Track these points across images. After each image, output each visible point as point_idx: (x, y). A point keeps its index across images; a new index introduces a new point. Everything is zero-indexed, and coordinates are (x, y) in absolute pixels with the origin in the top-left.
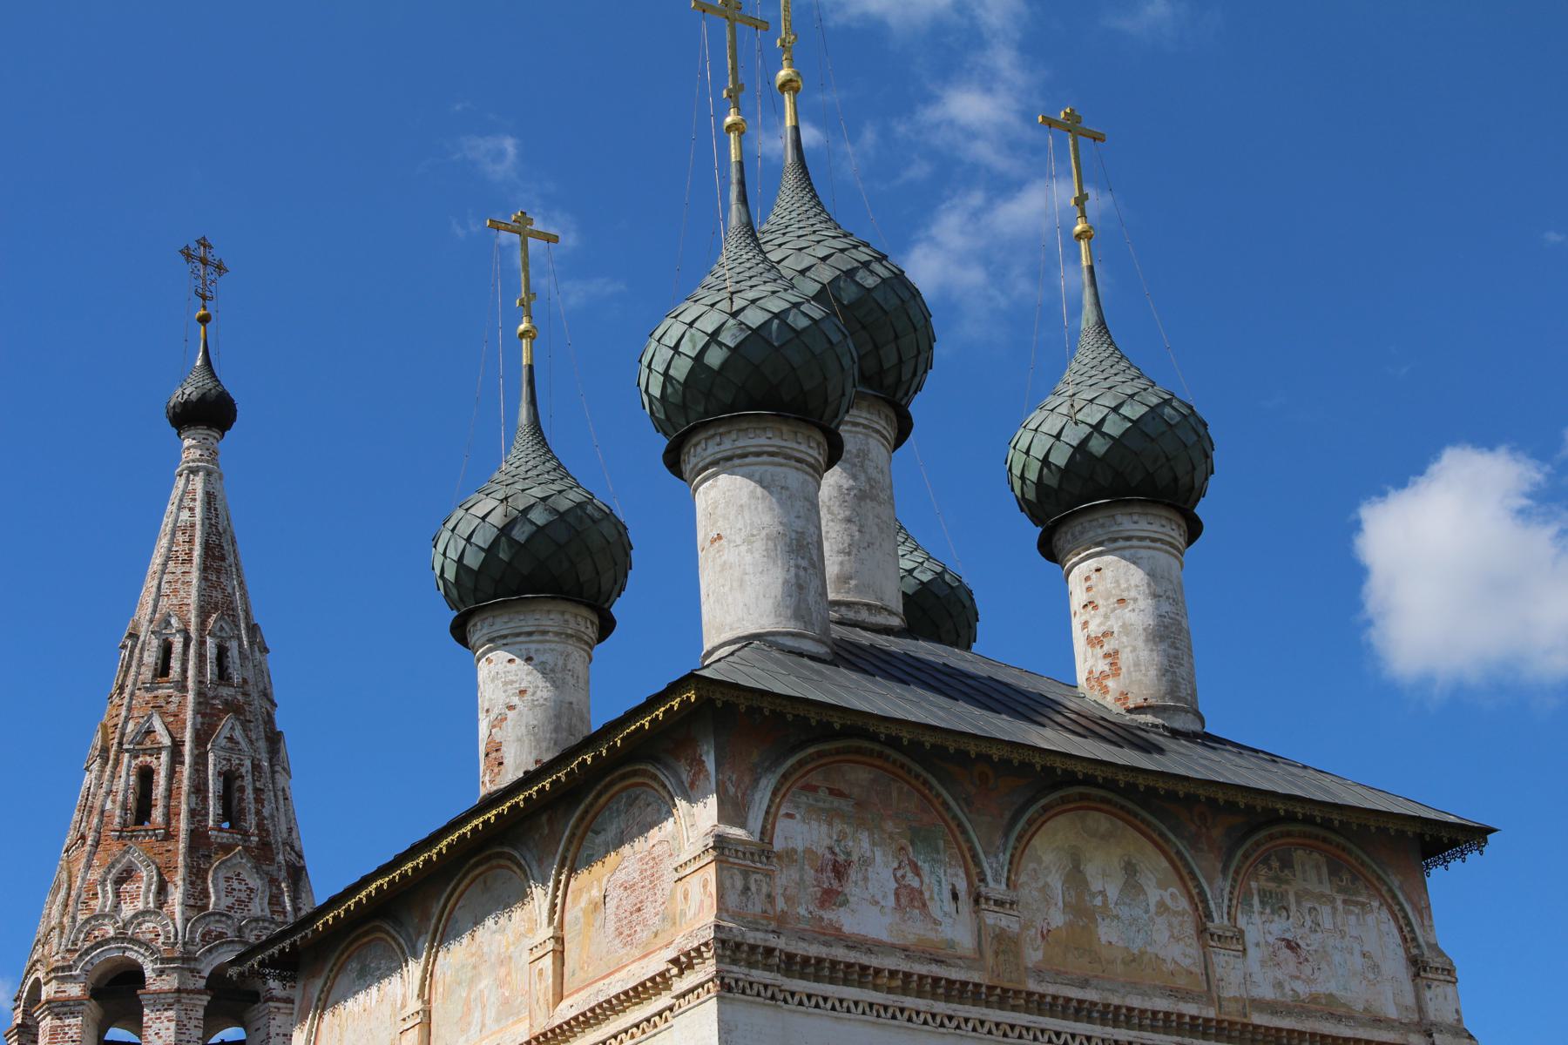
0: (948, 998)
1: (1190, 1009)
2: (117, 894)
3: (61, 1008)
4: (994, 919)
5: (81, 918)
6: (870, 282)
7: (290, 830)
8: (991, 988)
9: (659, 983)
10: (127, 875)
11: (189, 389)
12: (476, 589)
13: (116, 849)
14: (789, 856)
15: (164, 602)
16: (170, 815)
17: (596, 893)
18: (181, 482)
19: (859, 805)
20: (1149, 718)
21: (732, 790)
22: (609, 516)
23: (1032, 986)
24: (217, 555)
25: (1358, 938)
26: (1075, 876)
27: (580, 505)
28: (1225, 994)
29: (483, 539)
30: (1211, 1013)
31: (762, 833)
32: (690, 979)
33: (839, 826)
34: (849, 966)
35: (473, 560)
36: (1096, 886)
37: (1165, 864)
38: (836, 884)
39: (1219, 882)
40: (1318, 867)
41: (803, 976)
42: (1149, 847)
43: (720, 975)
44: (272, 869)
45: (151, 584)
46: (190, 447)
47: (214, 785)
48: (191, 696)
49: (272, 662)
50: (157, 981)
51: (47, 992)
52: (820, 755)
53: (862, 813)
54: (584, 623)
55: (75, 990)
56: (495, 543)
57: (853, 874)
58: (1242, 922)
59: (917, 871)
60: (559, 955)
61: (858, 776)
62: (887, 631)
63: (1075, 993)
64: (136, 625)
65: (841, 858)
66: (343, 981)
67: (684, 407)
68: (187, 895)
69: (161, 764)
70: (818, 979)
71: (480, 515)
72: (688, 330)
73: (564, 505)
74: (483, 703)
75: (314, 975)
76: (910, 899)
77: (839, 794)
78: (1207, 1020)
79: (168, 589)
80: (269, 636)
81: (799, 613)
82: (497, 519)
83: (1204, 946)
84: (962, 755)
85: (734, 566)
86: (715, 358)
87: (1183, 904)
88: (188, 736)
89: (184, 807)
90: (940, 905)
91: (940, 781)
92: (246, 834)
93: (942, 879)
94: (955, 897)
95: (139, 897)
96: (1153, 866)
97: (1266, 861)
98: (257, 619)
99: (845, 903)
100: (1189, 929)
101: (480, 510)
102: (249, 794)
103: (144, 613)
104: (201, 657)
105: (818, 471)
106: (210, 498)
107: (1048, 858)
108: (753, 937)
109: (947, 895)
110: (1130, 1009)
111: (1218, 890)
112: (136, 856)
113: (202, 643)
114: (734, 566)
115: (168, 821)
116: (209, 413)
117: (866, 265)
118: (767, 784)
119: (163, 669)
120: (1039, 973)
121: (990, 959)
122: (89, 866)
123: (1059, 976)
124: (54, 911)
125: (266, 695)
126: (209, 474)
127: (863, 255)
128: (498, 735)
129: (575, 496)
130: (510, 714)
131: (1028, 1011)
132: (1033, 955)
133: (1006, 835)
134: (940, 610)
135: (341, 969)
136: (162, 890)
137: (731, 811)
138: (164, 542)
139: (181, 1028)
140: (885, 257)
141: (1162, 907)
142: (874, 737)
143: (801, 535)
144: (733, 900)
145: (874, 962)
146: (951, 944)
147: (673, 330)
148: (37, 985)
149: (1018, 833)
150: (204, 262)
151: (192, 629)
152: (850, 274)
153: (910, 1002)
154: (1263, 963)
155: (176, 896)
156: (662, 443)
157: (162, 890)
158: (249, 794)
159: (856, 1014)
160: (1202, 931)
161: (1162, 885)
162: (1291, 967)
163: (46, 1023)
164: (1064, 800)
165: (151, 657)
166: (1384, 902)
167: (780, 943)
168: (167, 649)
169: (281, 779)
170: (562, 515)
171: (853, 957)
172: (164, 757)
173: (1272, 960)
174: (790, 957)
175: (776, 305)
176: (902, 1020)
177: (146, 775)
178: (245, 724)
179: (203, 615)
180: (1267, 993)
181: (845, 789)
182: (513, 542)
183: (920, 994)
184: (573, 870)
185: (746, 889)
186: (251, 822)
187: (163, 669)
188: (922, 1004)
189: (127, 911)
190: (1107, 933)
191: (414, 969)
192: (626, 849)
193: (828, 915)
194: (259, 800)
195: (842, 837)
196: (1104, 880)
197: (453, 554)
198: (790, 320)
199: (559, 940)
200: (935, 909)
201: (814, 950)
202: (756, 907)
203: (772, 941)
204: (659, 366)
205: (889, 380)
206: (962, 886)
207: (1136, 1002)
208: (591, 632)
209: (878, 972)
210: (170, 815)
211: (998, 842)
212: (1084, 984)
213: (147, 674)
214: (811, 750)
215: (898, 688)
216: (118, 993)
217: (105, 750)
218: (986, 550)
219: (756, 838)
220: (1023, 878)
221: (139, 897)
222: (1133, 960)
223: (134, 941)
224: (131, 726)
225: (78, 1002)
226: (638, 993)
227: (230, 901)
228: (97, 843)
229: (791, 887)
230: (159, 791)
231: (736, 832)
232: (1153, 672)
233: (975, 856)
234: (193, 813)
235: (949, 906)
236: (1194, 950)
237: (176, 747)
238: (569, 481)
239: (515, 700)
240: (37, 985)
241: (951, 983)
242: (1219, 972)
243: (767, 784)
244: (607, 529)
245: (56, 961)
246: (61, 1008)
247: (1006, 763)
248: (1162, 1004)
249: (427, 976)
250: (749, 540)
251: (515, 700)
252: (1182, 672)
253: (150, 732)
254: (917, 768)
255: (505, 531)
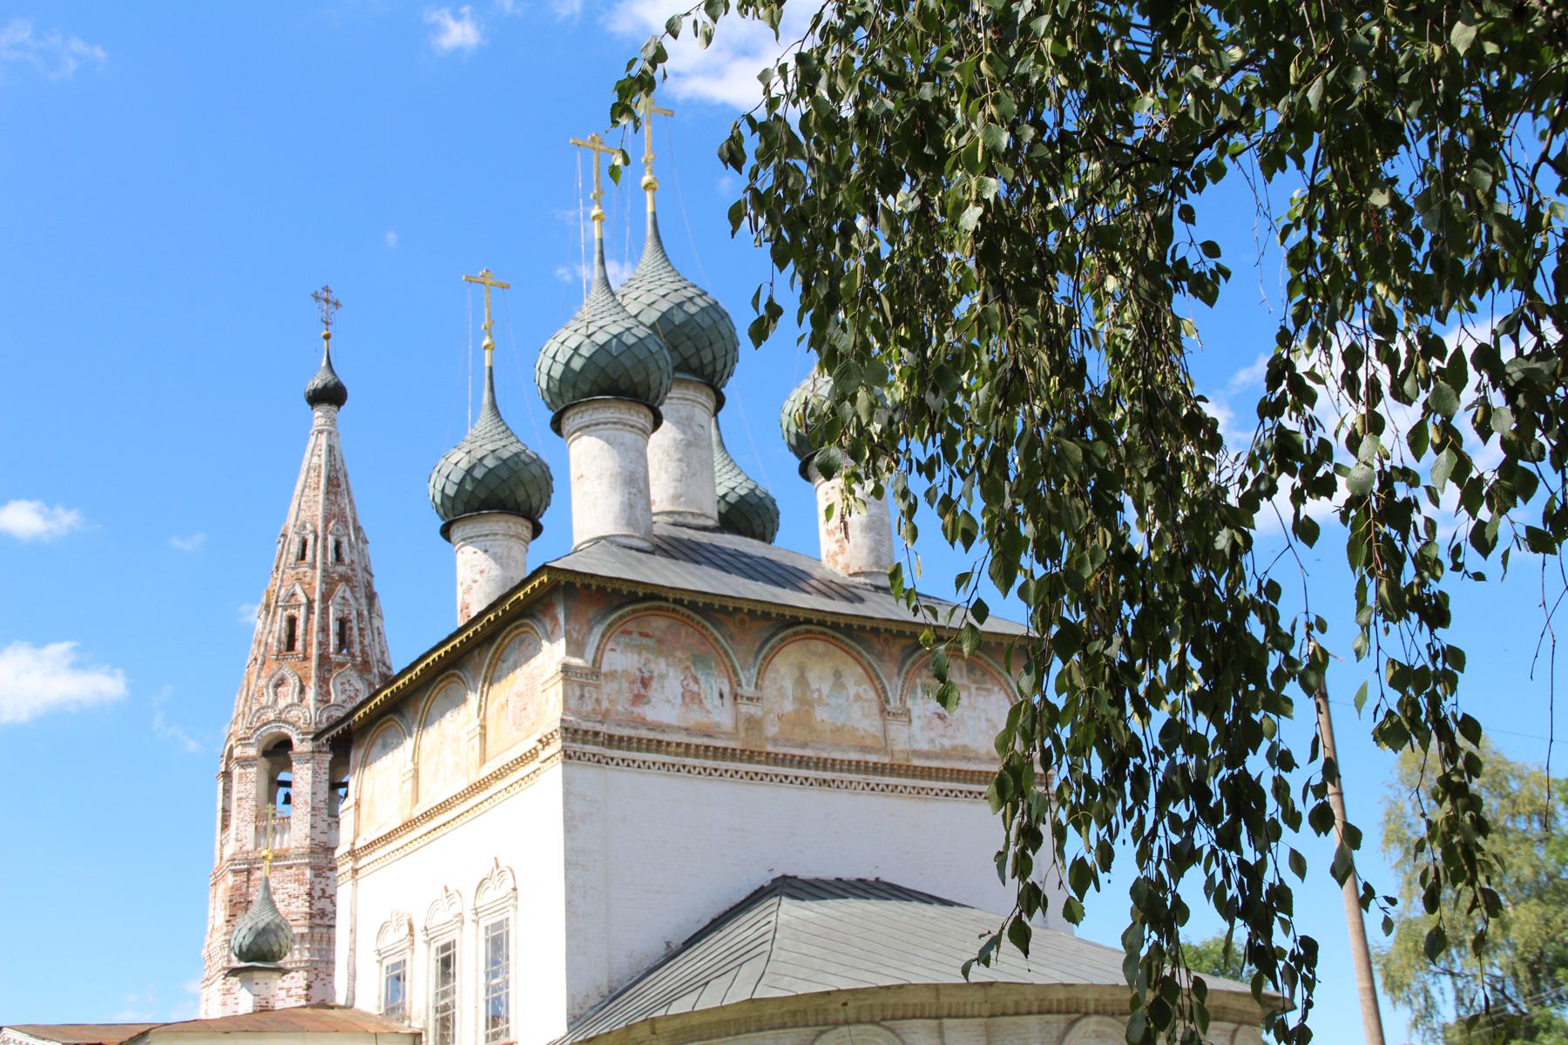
0: (715, 758)
1: (873, 758)
2: (276, 694)
3: (245, 762)
4: (746, 709)
5: (255, 708)
6: (693, 310)
7: (383, 653)
8: (743, 751)
9: (532, 755)
10: (281, 683)
11: (318, 381)
12: (453, 508)
13: (275, 666)
14: (612, 675)
15: (302, 514)
16: (306, 645)
17: (502, 699)
18: (313, 439)
19: (659, 641)
20: (862, 580)
21: (575, 635)
22: (537, 461)
23: (770, 748)
24: (335, 483)
25: (984, 710)
26: (801, 680)
27: (516, 454)
28: (897, 748)
29: (456, 477)
30: (886, 760)
31: (594, 661)
32: (549, 751)
33: (645, 655)
34: (650, 741)
35: (451, 491)
36: (814, 685)
37: (860, 670)
38: (643, 691)
39: (895, 679)
40: (960, 669)
41: (619, 748)
42: (850, 660)
43: (564, 749)
44: (370, 677)
45: (295, 503)
46: (319, 416)
47: (333, 627)
48: (319, 572)
49: (372, 550)
50: (301, 746)
51: (237, 752)
52: (634, 611)
53: (661, 647)
54: (524, 528)
55: (252, 752)
56: (463, 480)
57: (654, 684)
58: (909, 704)
59: (696, 680)
60: (483, 736)
61: (659, 624)
62: (705, 529)
63: (798, 752)
64: (286, 529)
65: (647, 675)
66: (375, 750)
67: (560, 395)
68: (318, 694)
69: (301, 614)
70: (629, 749)
71: (453, 465)
72: (564, 346)
73: (506, 454)
74: (460, 579)
75: (359, 747)
76: (691, 698)
77: (645, 635)
78: (884, 765)
79: (306, 506)
80: (368, 532)
81: (631, 522)
82: (464, 465)
83: (884, 720)
84: (723, 609)
85: (597, 494)
86: (577, 364)
87: (872, 694)
88: (317, 596)
89: (315, 641)
90: (712, 701)
91: (714, 625)
92: (353, 656)
93: (713, 684)
94: (721, 696)
95: (288, 694)
96: (853, 673)
97: (926, 666)
98: (361, 522)
99: (648, 702)
100: (875, 709)
101: (454, 459)
102: (356, 632)
103: (291, 521)
104: (325, 548)
105: (646, 434)
106: (331, 449)
107: (784, 670)
108: (585, 726)
109: (716, 695)
110: (834, 760)
111: (894, 686)
112: (286, 671)
113: (325, 539)
114: (597, 494)
115: (305, 650)
116: (331, 396)
117: (691, 299)
118: (598, 631)
119: (302, 556)
120: (775, 741)
121: (742, 734)
122: (259, 677)
123: (789, 742)
124: (239, 703)
125: (366, 570)
126: (330, 433)
127: (690, 292)
128: (468, 599)
129: (514, 449)
130: (475, 586)
131: (767, 764)
132: (772, 730)
133: (756, 657)
134: (749, 515)
135: (372, 744)
136: (302, 690)
137: (575, 647)
138: (302, 477)
139: (315, 773)
140: (705, 293)
141: (858, 697)
142: (666, 599)
143: (632, 473)
144: (573, 703)
145: (665, 737)
146: (718, 725)
147: (552, 346)
148: (231, 749)
149: (764, 659)
150: (327, 301)
151: (320, 534)
152: (680, 305)
153: (689, 761)
154: (922, 729)
155: (311, 694)
156: (551, 414)
157: (302, 690)
158: (356, 632)
159: (654, 769)
160: (883, 710)
161: (858, 683)
162: (941, 730)
163: (237, 771)
164: (796, 634)
165: (295, 548)
166: (1002, 687)
167: (603, 729)
168: (304, 544)
169: (376, 622)
170: (504, 461)
171: (651, 735)
172: (303, 609)
173: (929, 726)
174: (611, 737)
175: (615, 330)
176: (684, 772)
177: (292, 621)
178: (352, 589)
179: (327, 521)
180: (924, 746)
181: (650, 631)
182: (474, 479)
183: (697, 756)
184: (491, 684)
185: (582, 696)
186: (357, 649)
187: (302, 556)
188: (697, 762)
189: (282, 703)
190: (820, 714)
191: (409, 743)
192: (518, 671)
193: (638, 710)
194: (361, 635)
195: (647, 662)
196: (819, 679)
197: (439, 488)
198: (624, 338)
199: (483, 727)
200: (708, 704)
201: (626, 732)
202: (589, 706)
203: (598, 727)
204: (544, 370)
205: (708, 370)
206: (726, 689)
207: (838, 755)
208: (527, 533)
209: (668, 744)
210: (306, 645)
211: (750, 660)
212: (805, 745)
213: (292, 559)
214: (628, 609)
215: (691, 567)
216: (278, 751)
217: (268, 606)
218: (774, 472)
219: (589, 665)
220: (767, 683)
221: (288, 694)
222: (837, 730)
223: (285, 722)
224: (283, 592)
225: (254, 759)
226: (523, 760)
227: (344, 697)
228: (264, 663)
229: (614, 696)
230: (299, 631)
231: (576, 661)
232: (865, 551)
233: (735, 671)
234: (320, 644)
235: (718, 702)
236: (878, 722)
237: (310, 604)
238: (513, 439)
239: (478, 577)
240: (231, 749)
241: (716, 749)
242: (892, 735)
243: (598, 631)
244: (535, 469)
245: (241, 734)
246: (245, 762)
247: (751, 613)
248: (854, 756)
249: (416, 748)
250: (600, 477)
251: (478, 577)
252: (884, 550)
253: (293, 595)
254: (697, 618)
255: (469, 471)
